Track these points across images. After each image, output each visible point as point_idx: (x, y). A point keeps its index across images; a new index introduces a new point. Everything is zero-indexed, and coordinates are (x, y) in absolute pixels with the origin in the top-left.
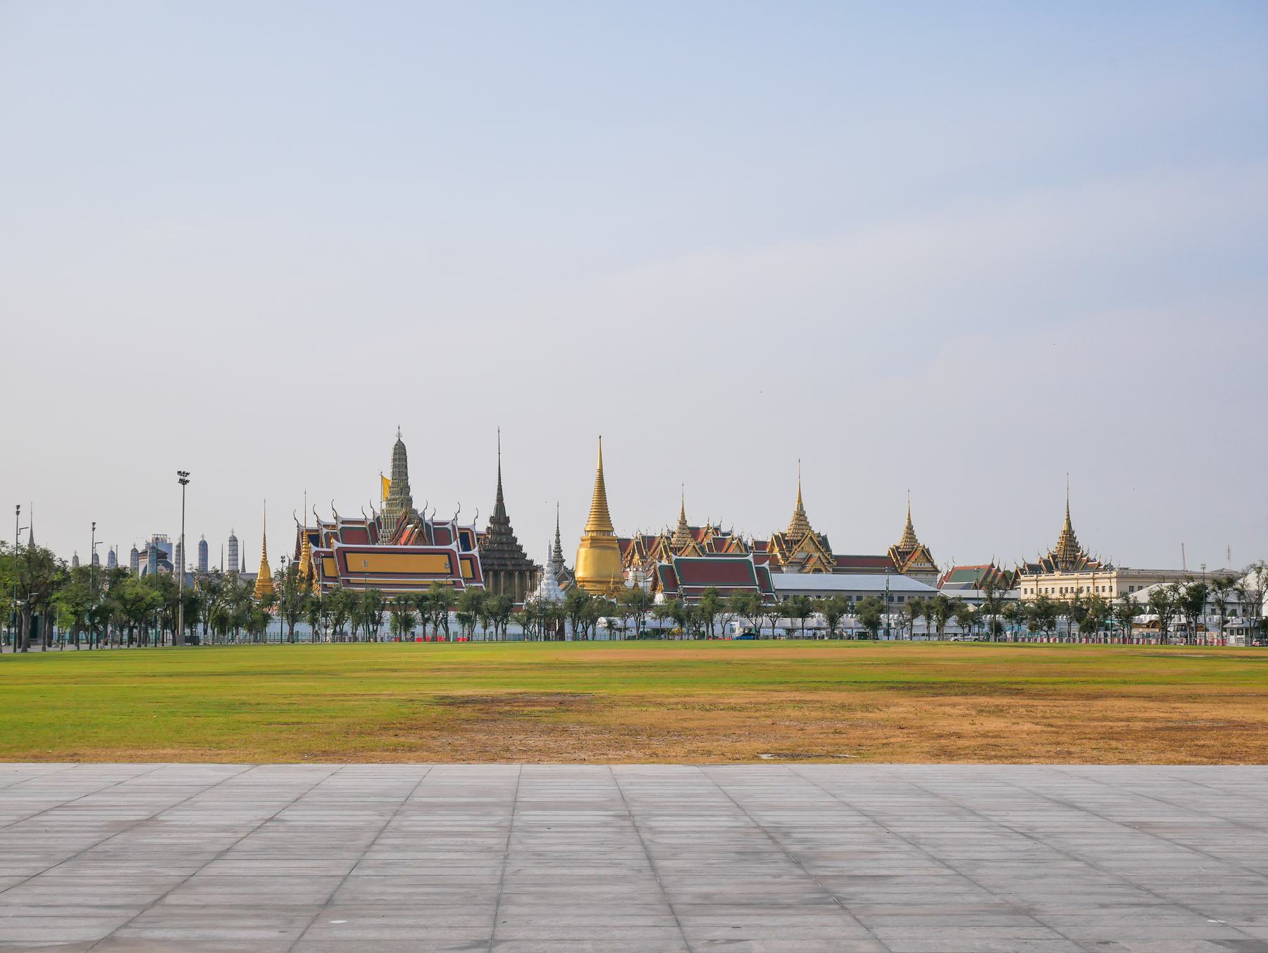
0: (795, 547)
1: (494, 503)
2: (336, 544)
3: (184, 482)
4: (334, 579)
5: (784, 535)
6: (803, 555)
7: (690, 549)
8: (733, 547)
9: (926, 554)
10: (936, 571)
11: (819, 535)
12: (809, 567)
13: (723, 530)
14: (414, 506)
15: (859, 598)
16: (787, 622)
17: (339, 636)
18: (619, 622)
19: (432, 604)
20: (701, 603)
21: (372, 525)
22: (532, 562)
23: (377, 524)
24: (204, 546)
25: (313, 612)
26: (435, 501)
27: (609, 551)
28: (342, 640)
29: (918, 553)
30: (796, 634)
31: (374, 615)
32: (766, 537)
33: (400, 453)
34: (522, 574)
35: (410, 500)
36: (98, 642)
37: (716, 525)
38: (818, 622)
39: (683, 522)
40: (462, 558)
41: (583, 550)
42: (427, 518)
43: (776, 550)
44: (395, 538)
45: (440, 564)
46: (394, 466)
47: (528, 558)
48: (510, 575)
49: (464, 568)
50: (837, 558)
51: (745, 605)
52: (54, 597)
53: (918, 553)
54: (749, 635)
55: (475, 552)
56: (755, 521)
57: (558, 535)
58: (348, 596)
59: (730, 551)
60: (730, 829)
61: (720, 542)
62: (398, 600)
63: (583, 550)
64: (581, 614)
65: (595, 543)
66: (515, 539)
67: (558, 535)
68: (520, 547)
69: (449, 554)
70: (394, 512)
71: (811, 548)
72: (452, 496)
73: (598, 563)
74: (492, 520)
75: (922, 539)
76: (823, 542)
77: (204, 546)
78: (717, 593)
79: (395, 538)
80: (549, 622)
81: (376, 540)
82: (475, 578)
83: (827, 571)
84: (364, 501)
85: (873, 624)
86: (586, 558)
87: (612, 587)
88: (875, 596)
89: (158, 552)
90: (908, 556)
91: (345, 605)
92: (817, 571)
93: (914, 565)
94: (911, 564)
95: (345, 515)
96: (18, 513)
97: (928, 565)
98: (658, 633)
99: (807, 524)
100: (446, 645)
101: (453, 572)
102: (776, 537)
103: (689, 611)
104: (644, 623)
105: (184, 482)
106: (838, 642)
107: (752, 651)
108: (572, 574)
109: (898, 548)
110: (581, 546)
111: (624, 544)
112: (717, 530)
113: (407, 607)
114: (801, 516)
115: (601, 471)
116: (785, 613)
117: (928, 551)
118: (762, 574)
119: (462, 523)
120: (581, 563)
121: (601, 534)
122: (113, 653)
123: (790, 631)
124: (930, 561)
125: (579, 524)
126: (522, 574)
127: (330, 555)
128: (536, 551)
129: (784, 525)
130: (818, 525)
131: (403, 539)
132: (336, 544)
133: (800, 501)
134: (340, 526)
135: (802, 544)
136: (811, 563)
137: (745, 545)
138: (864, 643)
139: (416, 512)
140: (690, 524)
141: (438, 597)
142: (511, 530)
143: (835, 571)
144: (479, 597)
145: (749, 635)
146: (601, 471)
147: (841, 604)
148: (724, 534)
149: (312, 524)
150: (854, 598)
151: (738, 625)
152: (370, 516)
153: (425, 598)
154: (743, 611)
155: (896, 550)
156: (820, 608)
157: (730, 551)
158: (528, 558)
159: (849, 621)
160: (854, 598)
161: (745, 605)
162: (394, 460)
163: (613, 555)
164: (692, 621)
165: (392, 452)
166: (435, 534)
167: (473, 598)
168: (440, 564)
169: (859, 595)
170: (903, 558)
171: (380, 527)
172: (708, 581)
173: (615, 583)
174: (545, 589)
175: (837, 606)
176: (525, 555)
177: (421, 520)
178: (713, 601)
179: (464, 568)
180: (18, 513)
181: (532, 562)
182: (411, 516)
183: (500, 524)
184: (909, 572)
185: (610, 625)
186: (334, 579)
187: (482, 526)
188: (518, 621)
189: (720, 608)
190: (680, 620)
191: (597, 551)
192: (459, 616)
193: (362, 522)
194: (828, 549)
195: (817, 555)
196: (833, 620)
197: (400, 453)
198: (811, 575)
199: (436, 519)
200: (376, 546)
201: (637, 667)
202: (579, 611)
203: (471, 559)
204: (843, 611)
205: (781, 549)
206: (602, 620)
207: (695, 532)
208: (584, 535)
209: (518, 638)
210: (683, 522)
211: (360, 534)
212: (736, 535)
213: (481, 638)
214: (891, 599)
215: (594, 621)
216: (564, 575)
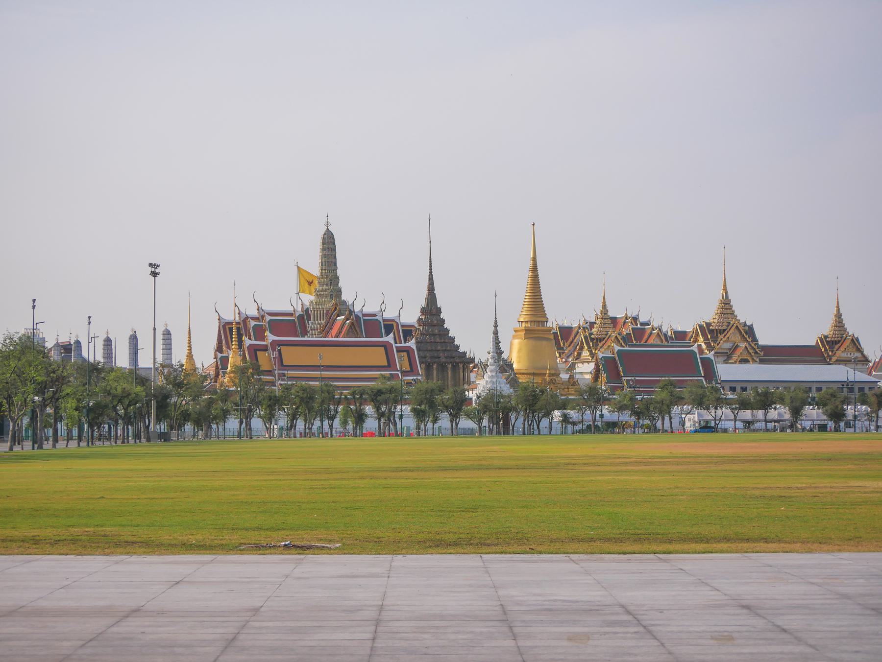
0: (721, 337)
1: (425, 293)
2: (270, 337)
3: (155, 274)
4: (270, 373)
5: (709, 325)
6: (728, 345)
8: (653, 337)
9: (855, 343)
10: (866, 360)
11: (745, 324)
12: (735, 357)
13: (642, 319)
14: (343, 298)
15: (819, 389)
16: (747, 414)
18: (573, 414)
19: (384, 398)
20: (660, 395)
21: (301, 317)
22: (465, 353)
23: (305, 316)
24: (134, 340)
26: (362, 293)
27: (544, 343)
29: (848, 342)
30: (757, 425)
32: (688, 327)
33: (329, 243)
34: (455, 367)
36: (80, 439)
37: (634, 314)
38: (780, 414)
39: (605, 311)
40: (399, 350)
41: (516, 342)
42: (357, 309)
43: (701, 339)
44: (326, 330)
46: (323, 256)
47: (461, 350)
48: (442, 367)
50: (765, 348)
51: (703, 396)
52: (64, 393)
53: (848, 342)
54: (706, 428)
55: (412, 344)
56: (677, 309)
57: (496, 326)
59: (650, 342)
61: (640, 331)
62: (353, 394)
63: (516, 342)
64: (538, 406)
65: (529, 334)
67: (496, 326)
69: (386, 346)
71: (737, 338)
72: (380, 288)
73: (533, 354)
74: (424, 311)
75: (852, 328)
76: (749, 332)
77: (134, 340)
78: (672, 384)
79: (326, 330)
80: (498, 415)
81: (305, 333)
82: (412, 371)
83: (754, 361)
84: (286, 297)
85: (837, 416)
86: (520, 350)
87: (547, 378)
88: (835, 386)
89: (66, 349)
90: (837, 344)
91: (302, 399)
92: (744, 361)
93: (844, 355)
94: (841, 354)
95: (268, 307)
96: (34, 307)
97: (858, 355)
98: (611, 426)
99: (733, 313)
100: (671, 435)
101: (390, 365)
102: (701, 327)
103: (647, 405)
104: (602, 416)
105: (155, 274)
106: (798, 435)
107: (710, 446)
108: (510, 366)
109: (826, 337)
110: (514, 337)
111: (566, 332)
112: (635, 319)
113: (363, 402)
114: (726, 304)
115: (534, 259)
116: (744, 405)
117: (857, 339)
118: (708, 365)
120: (516, 353)
121: (536, 327)
123: (748, 424)
124: (859, 350)
125: (514, 313)
126: (455, 367)
127: (265, 349)
128: (470, 337)
129: (709, 314)
130: (743, 314)
131: (334, 331)
132: (270, 337)
133: (725, 289)
134: (268, 318)
135: (729, 332)
136: (738, 353)
137: (665, 335)
138: (823, 435)
139: (345, 302)
140: (611, 314)
141: (391, 390)
142: (443, 321)
143: (762, 361)
145: (706, 428)
146: (534, 259)
147: (801, 395)
148: (642, 324)
150: (814, 389)
151: (692, 418)
153: (380, 392)
154: (700, 402)
155: (824, 340)
156: (782, 401)
157: (650, 342)
158: (461, 350)
159: (812, 413)
160: (814, 389)
161: (703, 396)
162: (323, 249)
163: (548, 347)
164: (648, 415)
165: (320, 241)
166: (370, 326)
167: (426, 392)
168: (378, 357)
169: (819, 385)
170: (831, 348)
171: (309, 319)
172: (652, 373)
173: (551, 375)
174: (480, 386)
175: (798, 397)
176: (458, 347)
177: (351, 312)
178: (671, 393)
180: (34, 307)
181: (465, 353)
182: (341, 307)
183: (432, 315)
184: (839, 362)
185: (566, 419)
186: (270, 373)
187: (411, 316)
189: (679, 400)
190: (638, 414)
192: (414, 410)
193: (291, 315)
194: (755, 339)
195: (743, 345)
196: (796, 412)
197: (329, 243)
198: (737, 365)
199: (366, 310)
200: (306, 339)
201: (830, 459)
202: (527, 404)
203: (408, 350)
204: (805, 403)
205: (706, 339)
206: (557, 413)
207: (614, 320)
208: (517, 326)
209: (469, 433)
210: (605, 311)
211: (290, 325)
212: (656, 325)
214: (851, 390)
215: (548, 414)
216: (505, 367)
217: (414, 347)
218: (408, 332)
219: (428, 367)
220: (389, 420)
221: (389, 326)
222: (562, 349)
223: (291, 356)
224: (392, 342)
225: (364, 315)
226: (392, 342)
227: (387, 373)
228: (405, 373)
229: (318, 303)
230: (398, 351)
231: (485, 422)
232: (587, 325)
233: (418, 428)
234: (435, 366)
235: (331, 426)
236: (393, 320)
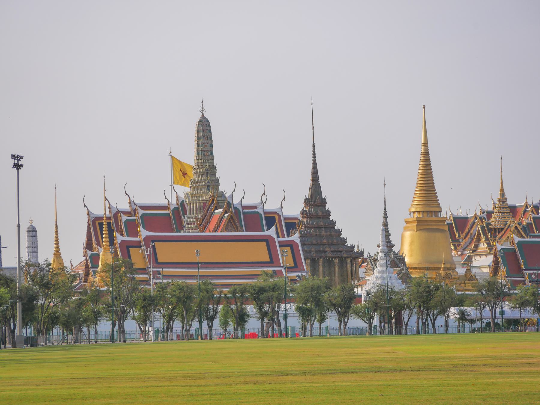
1: (308, 182)
3: (18, 167)
4: (144, 271)
7: (512, 229)
14: (221, 189)
17: (344, 331)
18: (471, 311)
19: (266, 297)
23: (181, 209)
25: (146, 308)
26: (242, 182)
27: (438, 235)
28: (237, 338)
31: (208, 309)
33: (204, 130)
35: (217, 182)
39: (503, 199)
40: (283, 245)
41: (408, 234)
42: (236, 201)
44: (203, 224)
45: (260, 252)
46: (198, 145)
47: (349, 243)
49: (284, 257)
55: (296, 238)
57: (385, 217)
58: (181, 289)
60: (324, 267)
62: (234, 292)
63: (408, 234)
66: (333, 223)
67: (385, 217)
68: (339, 232)
69: (268, 240)
70: (201, 195)
72: (261, 177)
73: (426, 247)
74: (307, 202)
79: (203, 224)
80: (389, 313)
81: (180, 227)
82: (297, 267)
86: (412, 243)
87: (442, 273)
95: (140, 200)
98: (514, 324)
101: (273, 260)
104: (502, 313)
105: (18, 167)
108: (402, 260)
110: (406, 229)
111: (461, 223)
115: (426, 145)
119: (268, 207)
121: (429, 217)
122: (11, 356)
125: (405, 204)
126: (342, 262)
127: (138, 245)
128: (359, 232)
131: (212, 225)
132: (144, 233)
134: (141, 212)
139: (222, 194)
141: (275, 288)
142: (328, 213)
144: (319, 287)
146: (426, 145)
149: (100, 211)
152: (174, 202)
153: (262, 290)
158: (349, 243)
162: (198, 138)
163: (442, 239)
166: (250, 220)
167: (312, 289)
168: (260, 252)
171: (185, 213)
173: (446, 269)
174: (370, 282)
176: (345, 240)
177: (230, 205)
179: (284, 257)
181: (352, 247)
182: (219, 200)
183: (316, 206)
185: (463, 317)
186: (144, 271)
187: (294, 208)
188: (358, 314)
191: (424, 234)
192: (299, 309)
193: (165, 208)
197: (204, 130)
199: (245, 202)
200: (182, 234)
202: (419, 302)
203: (291, 245)
206: (453, 310)
207: (513, 209)
208: (408, 217)
209: (360, 332)
210: (503, 199)
211: (164, 220)
213: (456, 331)
216: (396, 261)
217: (298, 241)
218: (291, 225)
219: (314, 262)
220: (273, 320)
221: (271, 219)
222: (457, 241)
223: (165, 253)
224: (274, 236)
225: (244, 208)
226: (274, 236)
227: (269, 270)
228: (289, 269)
229: (194, 195)
230: (280, 246)
231: (376, 321)
232: (484, 215)
233: (304, 328)
234: (321, 261)
235: (210, 328)
236: (275, 213)
